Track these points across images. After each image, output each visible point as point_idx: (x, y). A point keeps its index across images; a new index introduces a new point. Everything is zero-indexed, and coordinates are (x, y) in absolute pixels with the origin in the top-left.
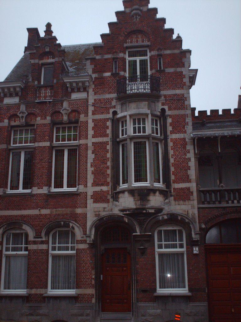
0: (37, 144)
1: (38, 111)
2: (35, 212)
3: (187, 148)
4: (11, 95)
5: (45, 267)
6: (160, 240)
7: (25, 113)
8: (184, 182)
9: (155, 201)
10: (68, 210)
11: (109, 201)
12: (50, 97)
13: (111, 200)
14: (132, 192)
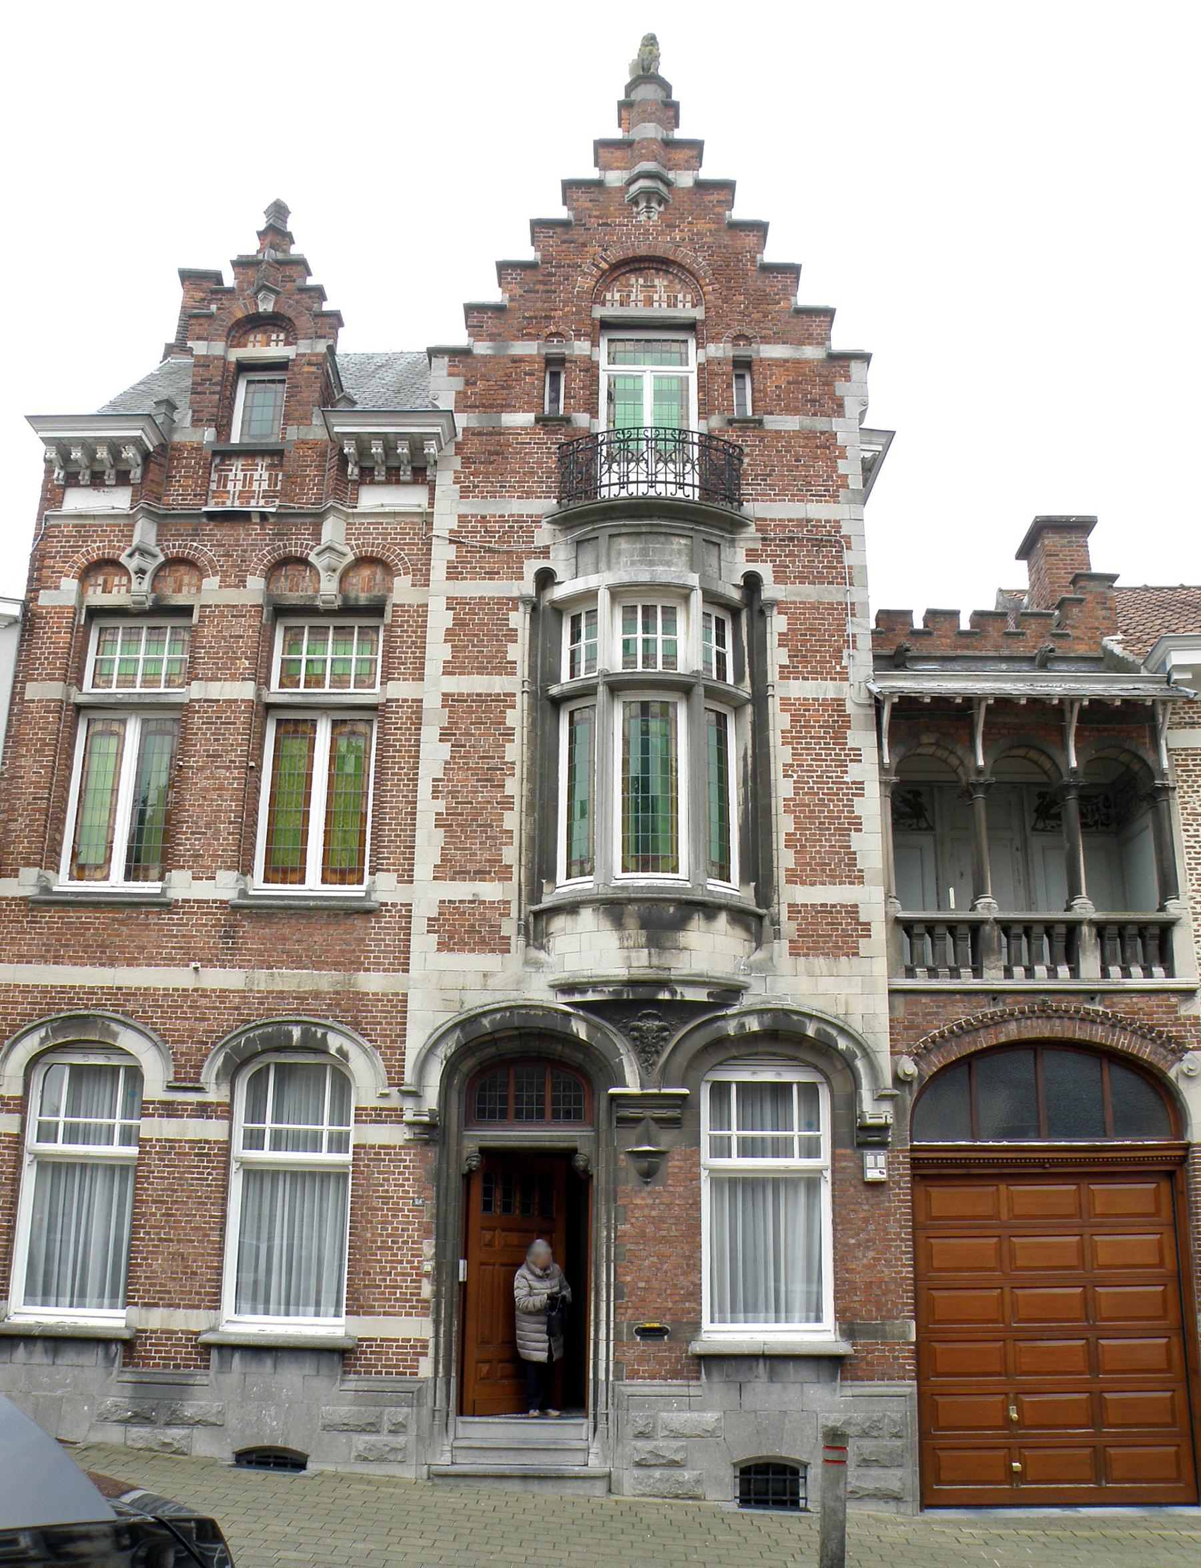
0: (196, 690)
1: (205, 549)
2: (178, 978)
3: (851, 743)
4: (97, 481)
5: (211, 1217)
6: (719, 1120)
7: (154, 556)
8: (834, 879)
9: (709, 951)
10: (324, 980)
11: (509, 944)
12: (268, 496)
13: (517, 942)
14: (614, 908)
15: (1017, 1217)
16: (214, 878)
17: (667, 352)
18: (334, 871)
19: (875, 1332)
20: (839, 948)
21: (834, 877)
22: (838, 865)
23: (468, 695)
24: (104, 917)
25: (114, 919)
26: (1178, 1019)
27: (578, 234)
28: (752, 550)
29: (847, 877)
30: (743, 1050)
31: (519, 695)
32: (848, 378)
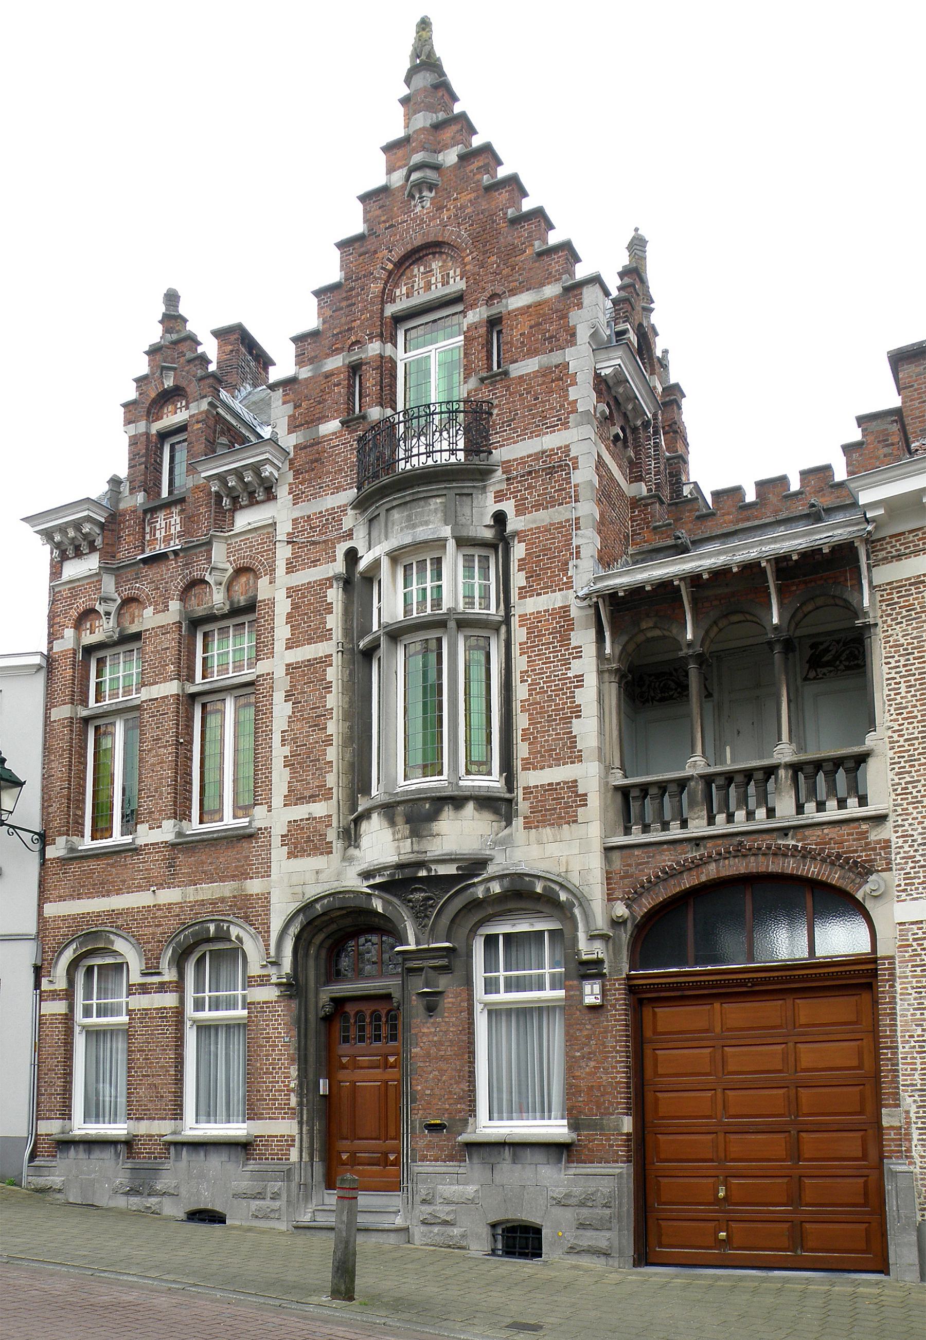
1: (143, 588)
3: (574, 643)
6: (490, 965)
7: (115, 600)
8: (559, 761)
9: (459, 834)
10: (226, 889)
11: (332, 847)
13: (337, 845)
14: (388, 809)
15: (729, 1030)
16: (161, 827)
17: (449, 327)
18: (240, 808)
19: (594, 1126)
20: (561, 818)
21: (558, 759)
22: (562, 749)
23: (302, 662)
24: (103, 863)
25: (108, 864)
26: (867, 844)
27: (370, 245)
28: (498, 492)
29: (569, 758)
30: (498, 909)
31: (334, 655)
32: (580, 305)
